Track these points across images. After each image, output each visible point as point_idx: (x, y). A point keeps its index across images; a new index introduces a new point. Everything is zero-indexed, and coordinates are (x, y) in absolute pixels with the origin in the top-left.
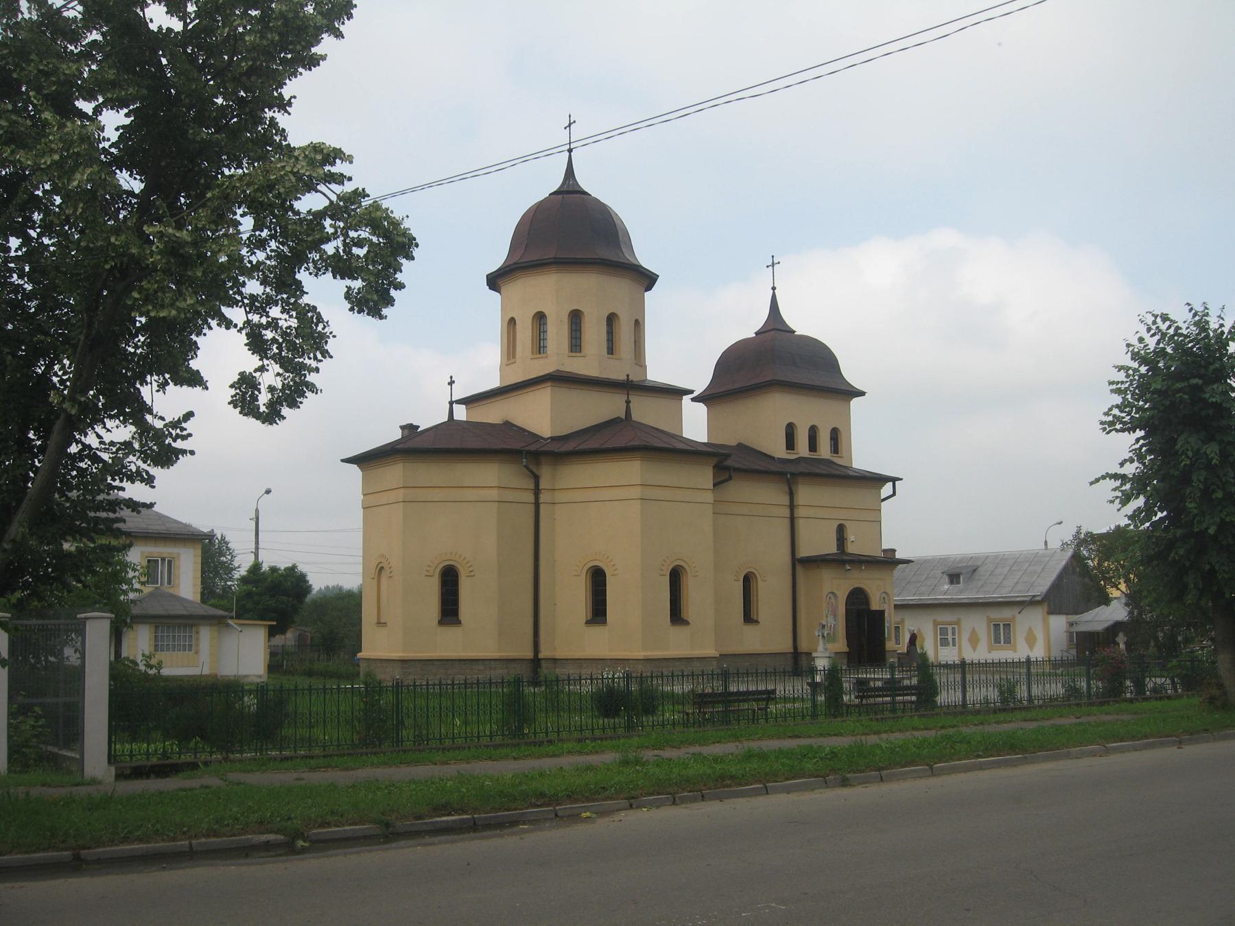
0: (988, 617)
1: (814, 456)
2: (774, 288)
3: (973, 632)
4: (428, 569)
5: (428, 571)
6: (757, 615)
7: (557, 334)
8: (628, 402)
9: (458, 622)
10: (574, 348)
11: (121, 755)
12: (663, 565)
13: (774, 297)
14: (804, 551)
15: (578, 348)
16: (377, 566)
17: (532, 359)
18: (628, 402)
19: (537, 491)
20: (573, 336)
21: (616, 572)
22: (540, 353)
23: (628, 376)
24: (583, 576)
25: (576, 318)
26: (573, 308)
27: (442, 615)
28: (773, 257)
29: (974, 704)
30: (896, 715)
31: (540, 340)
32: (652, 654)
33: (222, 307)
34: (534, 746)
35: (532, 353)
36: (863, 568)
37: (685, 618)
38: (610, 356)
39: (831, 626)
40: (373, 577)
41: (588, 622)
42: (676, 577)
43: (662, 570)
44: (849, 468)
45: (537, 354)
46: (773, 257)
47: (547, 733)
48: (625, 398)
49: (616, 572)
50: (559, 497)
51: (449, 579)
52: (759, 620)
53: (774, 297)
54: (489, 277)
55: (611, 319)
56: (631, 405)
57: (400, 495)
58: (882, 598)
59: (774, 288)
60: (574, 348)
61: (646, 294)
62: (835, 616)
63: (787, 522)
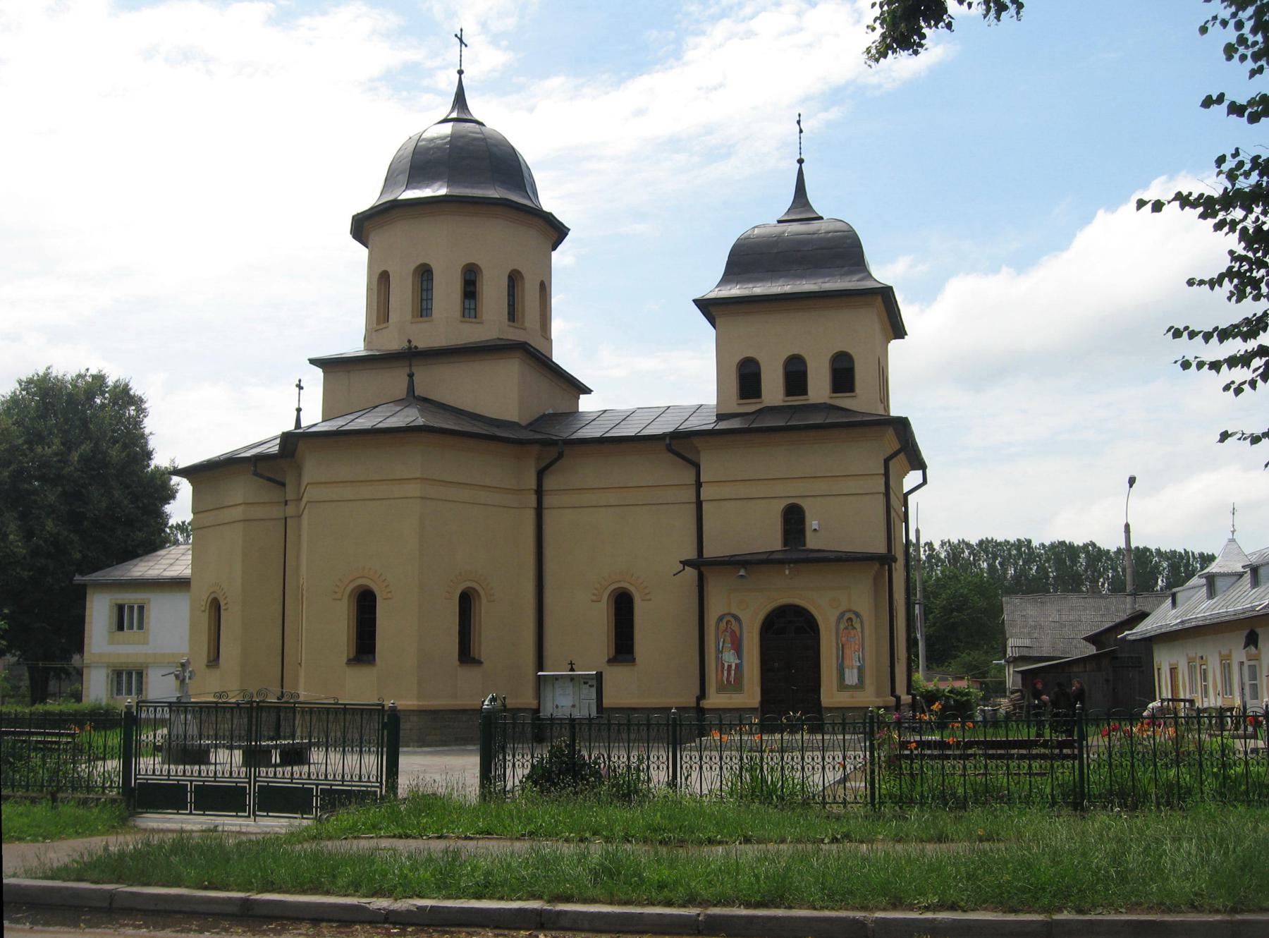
1: (797, 401)
2: (801, 161)
4: (595, 592)
7: (447, 291)
8: (411, 376)
9: (633, 660)
10: (467, 311)
12: (338, 586)
13: (800, 173)
14: (707, 554)
17: (412, 323)
18: (411, 376)
19: (699, 485)
20: (424, 297)
21: (389, 595)
22: (421, 316)
23: (409, 341)
25: (424, 274)
27: (356, 652)
31: (422, 300)
32: (431, 703)
33: (1217, 285)
34: (1105, 807)
35: (413, 316)
36: (787, 572)
37: (477, 657)
38: (511, 324)
39: (730, 666)
40: (203, 608)
41: (610, 661)
42: (467, 601)
43: (336, 592)
45: (417, 317)
46: (799, 115)
48: (407, 371)
49: (389, 595)
51: (365, 603)
52: (482, 660)
53: (800, 173)
54: (355, 218)
55: (514, 279)
57: (413, 490)
58: (846, 617)
59: (801, 161)
60: (467, 311)
61: (553, 253)
62: (738, 647)
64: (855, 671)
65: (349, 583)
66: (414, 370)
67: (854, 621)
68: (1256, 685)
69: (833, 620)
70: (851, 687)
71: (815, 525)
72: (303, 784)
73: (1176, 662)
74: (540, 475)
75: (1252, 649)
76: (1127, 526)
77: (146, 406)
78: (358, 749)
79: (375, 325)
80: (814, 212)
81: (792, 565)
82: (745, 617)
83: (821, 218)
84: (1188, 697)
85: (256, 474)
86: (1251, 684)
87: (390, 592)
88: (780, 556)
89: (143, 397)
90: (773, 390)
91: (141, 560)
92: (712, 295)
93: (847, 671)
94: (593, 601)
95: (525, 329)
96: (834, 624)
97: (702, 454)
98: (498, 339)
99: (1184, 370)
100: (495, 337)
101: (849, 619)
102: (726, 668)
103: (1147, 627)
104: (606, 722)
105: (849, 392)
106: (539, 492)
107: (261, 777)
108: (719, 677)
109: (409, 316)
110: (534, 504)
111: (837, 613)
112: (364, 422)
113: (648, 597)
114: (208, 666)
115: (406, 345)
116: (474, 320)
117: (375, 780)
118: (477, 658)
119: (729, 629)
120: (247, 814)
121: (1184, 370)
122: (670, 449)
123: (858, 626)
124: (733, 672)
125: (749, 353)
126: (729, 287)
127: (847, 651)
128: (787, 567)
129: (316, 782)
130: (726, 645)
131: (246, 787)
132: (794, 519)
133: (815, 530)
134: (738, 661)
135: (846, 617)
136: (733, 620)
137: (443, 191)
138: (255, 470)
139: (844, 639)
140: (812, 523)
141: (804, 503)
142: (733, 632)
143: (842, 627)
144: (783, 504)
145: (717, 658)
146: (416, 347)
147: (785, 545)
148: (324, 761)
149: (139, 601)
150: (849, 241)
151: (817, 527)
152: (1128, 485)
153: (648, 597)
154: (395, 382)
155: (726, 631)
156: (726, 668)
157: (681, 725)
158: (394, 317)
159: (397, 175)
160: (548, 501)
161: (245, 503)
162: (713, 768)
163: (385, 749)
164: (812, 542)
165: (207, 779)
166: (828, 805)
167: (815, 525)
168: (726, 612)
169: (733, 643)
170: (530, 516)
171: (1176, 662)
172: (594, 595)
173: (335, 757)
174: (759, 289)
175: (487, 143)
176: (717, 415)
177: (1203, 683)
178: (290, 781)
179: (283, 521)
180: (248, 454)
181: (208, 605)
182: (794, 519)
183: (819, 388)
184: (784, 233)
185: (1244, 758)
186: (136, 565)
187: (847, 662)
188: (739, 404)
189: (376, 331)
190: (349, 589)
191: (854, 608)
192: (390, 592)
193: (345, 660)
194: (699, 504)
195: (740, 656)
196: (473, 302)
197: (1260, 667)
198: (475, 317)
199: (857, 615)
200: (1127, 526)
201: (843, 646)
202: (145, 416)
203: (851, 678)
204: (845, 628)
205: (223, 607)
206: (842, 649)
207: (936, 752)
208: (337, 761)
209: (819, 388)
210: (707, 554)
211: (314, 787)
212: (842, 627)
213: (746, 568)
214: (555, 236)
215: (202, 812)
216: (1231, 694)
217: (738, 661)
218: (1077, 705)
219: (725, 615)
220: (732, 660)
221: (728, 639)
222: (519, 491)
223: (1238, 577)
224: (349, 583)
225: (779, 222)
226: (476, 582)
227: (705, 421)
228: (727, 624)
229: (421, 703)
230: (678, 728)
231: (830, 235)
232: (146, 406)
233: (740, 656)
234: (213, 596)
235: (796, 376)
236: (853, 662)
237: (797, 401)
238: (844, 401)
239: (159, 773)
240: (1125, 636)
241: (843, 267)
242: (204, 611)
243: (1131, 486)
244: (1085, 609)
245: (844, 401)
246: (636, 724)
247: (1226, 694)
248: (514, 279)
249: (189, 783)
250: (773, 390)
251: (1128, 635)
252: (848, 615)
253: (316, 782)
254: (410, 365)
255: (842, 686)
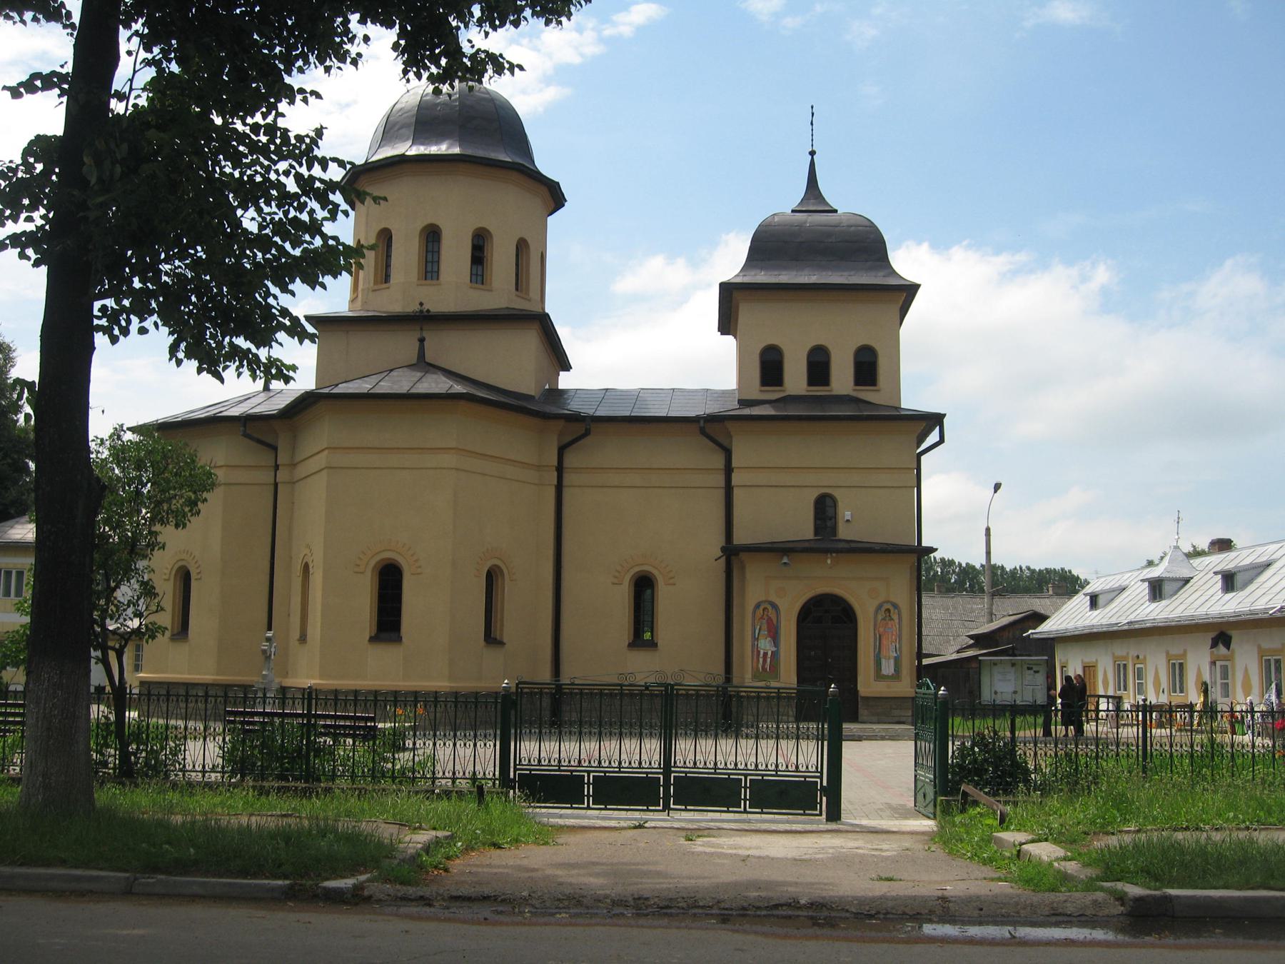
0: (1259, 647)
1: (819, 391)
2: (812, 153)
3: (1246, 670)
4: (617, 574)
5: (615, 577)
6: (502, 630)
7: (456, 255)
8: (422, 340)
10: (474, 277)
11: (482, 779)
12: (360, 559)
14: (740, 538)
15: (435, 275)
16: (178, 561)
18: (422, 340)
19: (728, 470)
21: (419, 571)
23: (421, 304)
24: (369, 573)
25: (432, 236)
26: (480, 226)
28: (812, 107)
29: (204, 772)
30: (1031, 799)
32: (245, 678)
35: (418, 279)
36: (829, 561)
39: (765, 654)
40: (166, 577)
44: (898, 408)
45: (381, 283)
46: (812, 107)
47: (454, 779)
48: (417, 335)
50: (301, 471)
52: (505, 641)
55: (522, 246)
56: (426, 343)
58: (883, 609)
59: (812, 153)
62: (774, 635)
63: (720, 495)
64: (892, 662)
65: (373, 556)
66: (425, 334)
67: (892, 611)
68: (1227, 684)
69: (872, 610)
70: (887, 677)
71: (848, 515)
72: (729, 774)
73: (1094, 660)
74: (561, 451)
75: (1222, 650)
76: (988, 530)
77: (14, 354)
78: (537, 731)
79: (372, 284)
80: (827, 204)
81: (834, 555)
82: (783, 604)
83: (836, 211)
84: (1111, 693)
85: (246, 435)
86: (1222, 683)
87: (420, 567)
88: (813, 545)
89: (11, 345)
90: (795, 379)
91: (17, 522)
92: (739, 280)
93: (883, 661)
94: (613, 584)
95: (529, 300)
96: (871, 615)
97: (734, 440)
98: (507, 308)
99: (722, 285)
100: (504, 306)
101: (887, 610)
102: (761, 655)
103: (1047, 628)
104: (393, 699)
105: (776, 385)
106: (560, 469)
107: (678, 767)
108: (755, 665)
109: (415, 279)
110: (555, 482)
111: (876, 603)
112: (385, 387)
113: (671, 581)
114: (373, 640)
115: (416, 308)
116: (481, 286)
117: (814, 769)
118: (498, 638)
119: (765, 617)
120: (818, 812)
121: (722, 285)
122: (703, 432)
123: (895, 617)
124: (769, 660)
125: (864, 341)
126: (753, 273)
127: (884, 642)
128: (829, 555)
129: (745, 772)
130: (762, 632)
131: (750, 808)
132: (825, 508)
133: (848, 521)
134: (774, 649)
135: (883, 609)
136: (769, 607)
137: (457, 150)
138: (245, 431)
139: (881, 630)
140: (845, 513)
141: (836, 493)
142: (770, 621)
143: (880, 617)
144: (815, 494)
145: (753, 645)
146: (428, 311)
147: (816, 534)
148: (754, 751)
149: (19, 566)
150: (872, 236)
151: (849, 518)
152: (993, 490)
153: (671, 581)
154: (403, 345)
155: (762, 618)
156: (761, 655)
157: (317, 699)
158: (397, 276)
159: (399, 129)
160: (568, 478)
161: (227, 466)
162: (467, 745)
163: (826, 743)
164: (844, 533)
165: (649, 770)
166: (458, 781)
167: (848, 515)
168: (764, 599)
169: (769, 631)
170: (551, 492)
171: (1094, 660)
172: (615, 577)
173: (706, 745)
174: (785, 277)
175: (495, 104)
176: (739, 400)
177: (1143, 681)
178: (713, 771)
179: (272, 488)
180: (235, 412)
181: (174, 572)
182: (825, 508)
183: (842, 380)
184: (805, 222)
185: (1230, 751)
186: (12, 527)
187: (884, 653)
188: (761, 391)
189: (373, 291)
190: (373, 563)
191: (892, 599)
192: (420, 567)
193: (368, 638)
194: (276, 485)
195: (776, 643)
196: (480, 268)
197: (1233, 667)
198: (483, 283)
199: (895, 606)
200: (988, 530)
201: (880, 636)
202: (12, 366)
203: (888, 668)
204: (882, 619)
205: (193, 576)
206: (879, 639)
207: (674, 731)
208: (770, 750)
209: (842, 380)
210: (740, 538)
211: (743, 778)
212: (880, 617)
213: (788, 556)
214: (553, 205)
215: (760, 810)
216: (1182, 691)
217: (774, 649)
218: (941, 692)
219: (762, 602)
220: (768, 648)
221: (765, 626)
222: (539, 468)
223: (1181, 583)
224: (373, 556)
225: (793, 211)
226: (500, 559)
227: (731, 406)
228: (763, 610)
229: (452, 685)
230: (314, 701)
231: (853, 228)
232: (14, 354)
233: (776, 643)
234: (180, 564)
235: (819, 367)
236: (890, 652)
237: (819, 391)
238: (867, 394)
239: (527, 762)
240: (1029, 635)
241: (867, 261)
242: (168, 580)
243: (995, 492)
244: (934, 608)
245: (867, 394)
246: (194, 696)
247: (1120, 690)
248: (522, 246)
249: (586, 774)
250: (795, 379)
251: (1032, 633)
252: (888, 606)
253: (745, 772)
254: (421, 329)
255: (879, 676)
